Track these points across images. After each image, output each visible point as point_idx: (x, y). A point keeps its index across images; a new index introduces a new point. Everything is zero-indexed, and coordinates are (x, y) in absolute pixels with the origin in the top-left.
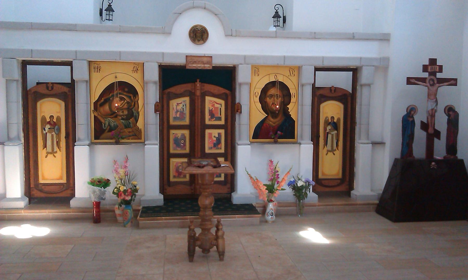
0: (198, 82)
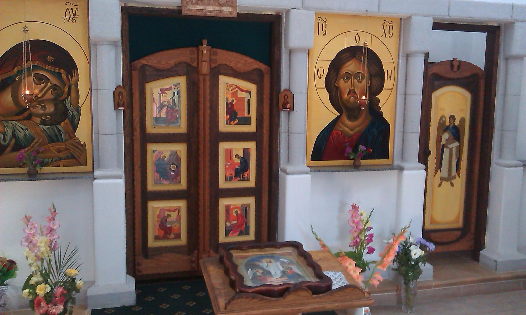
0: (205, 45)
